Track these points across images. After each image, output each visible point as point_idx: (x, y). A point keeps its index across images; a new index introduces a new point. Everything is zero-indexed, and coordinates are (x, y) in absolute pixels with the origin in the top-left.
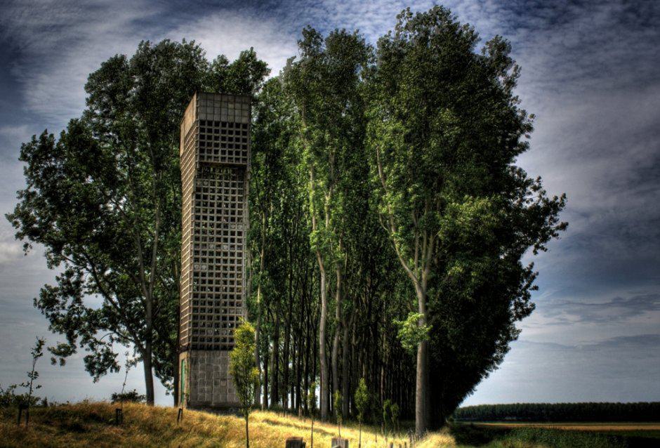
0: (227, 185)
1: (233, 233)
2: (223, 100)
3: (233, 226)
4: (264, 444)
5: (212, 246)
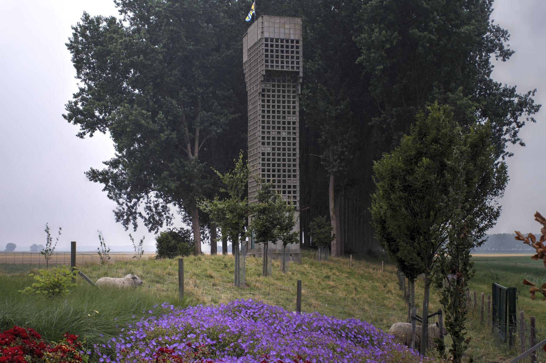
0: (284, 86)
2: (281, 21)
3: (289, 118)
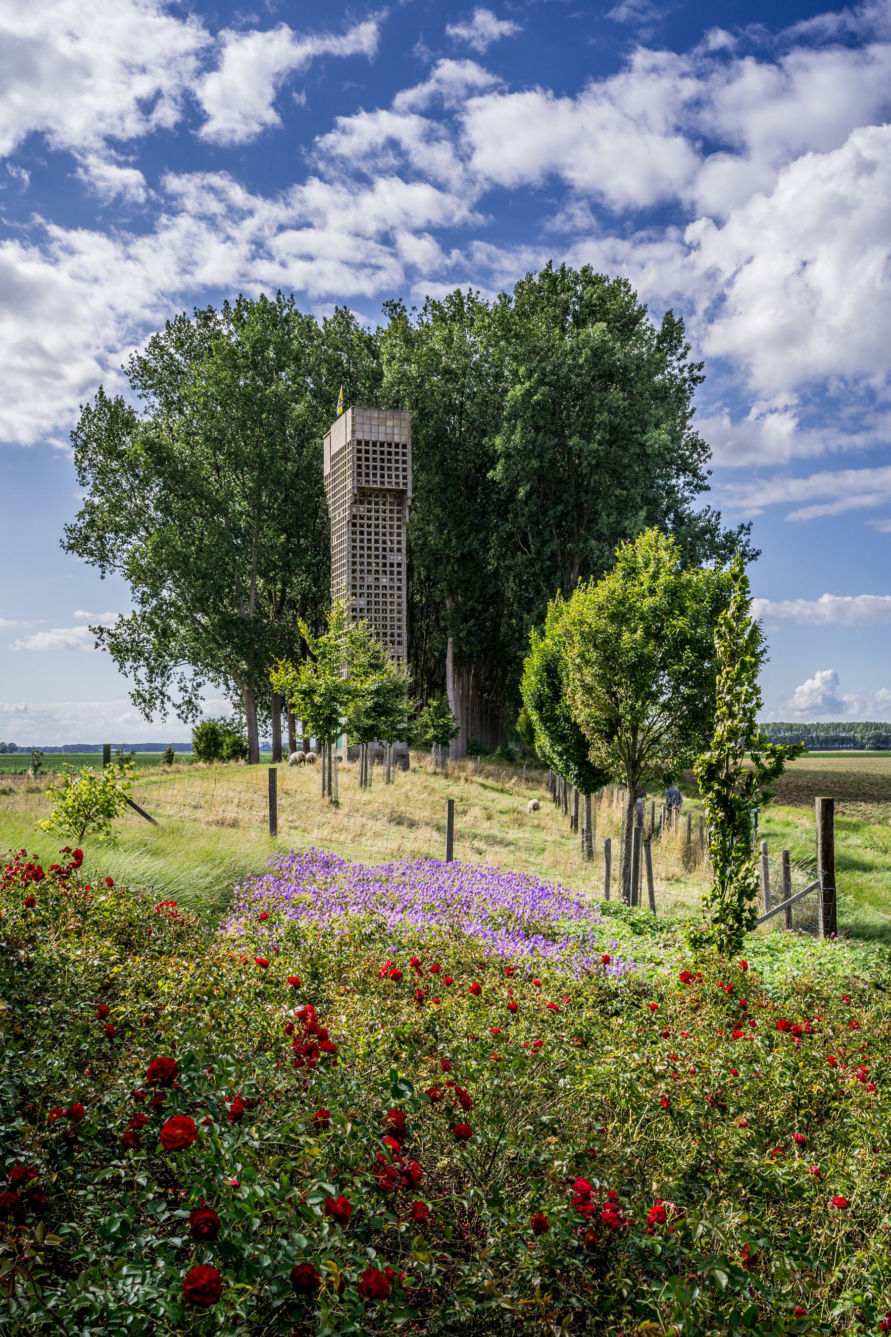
1: (392, 565)
4: (886, 969)
5: (370, 580)
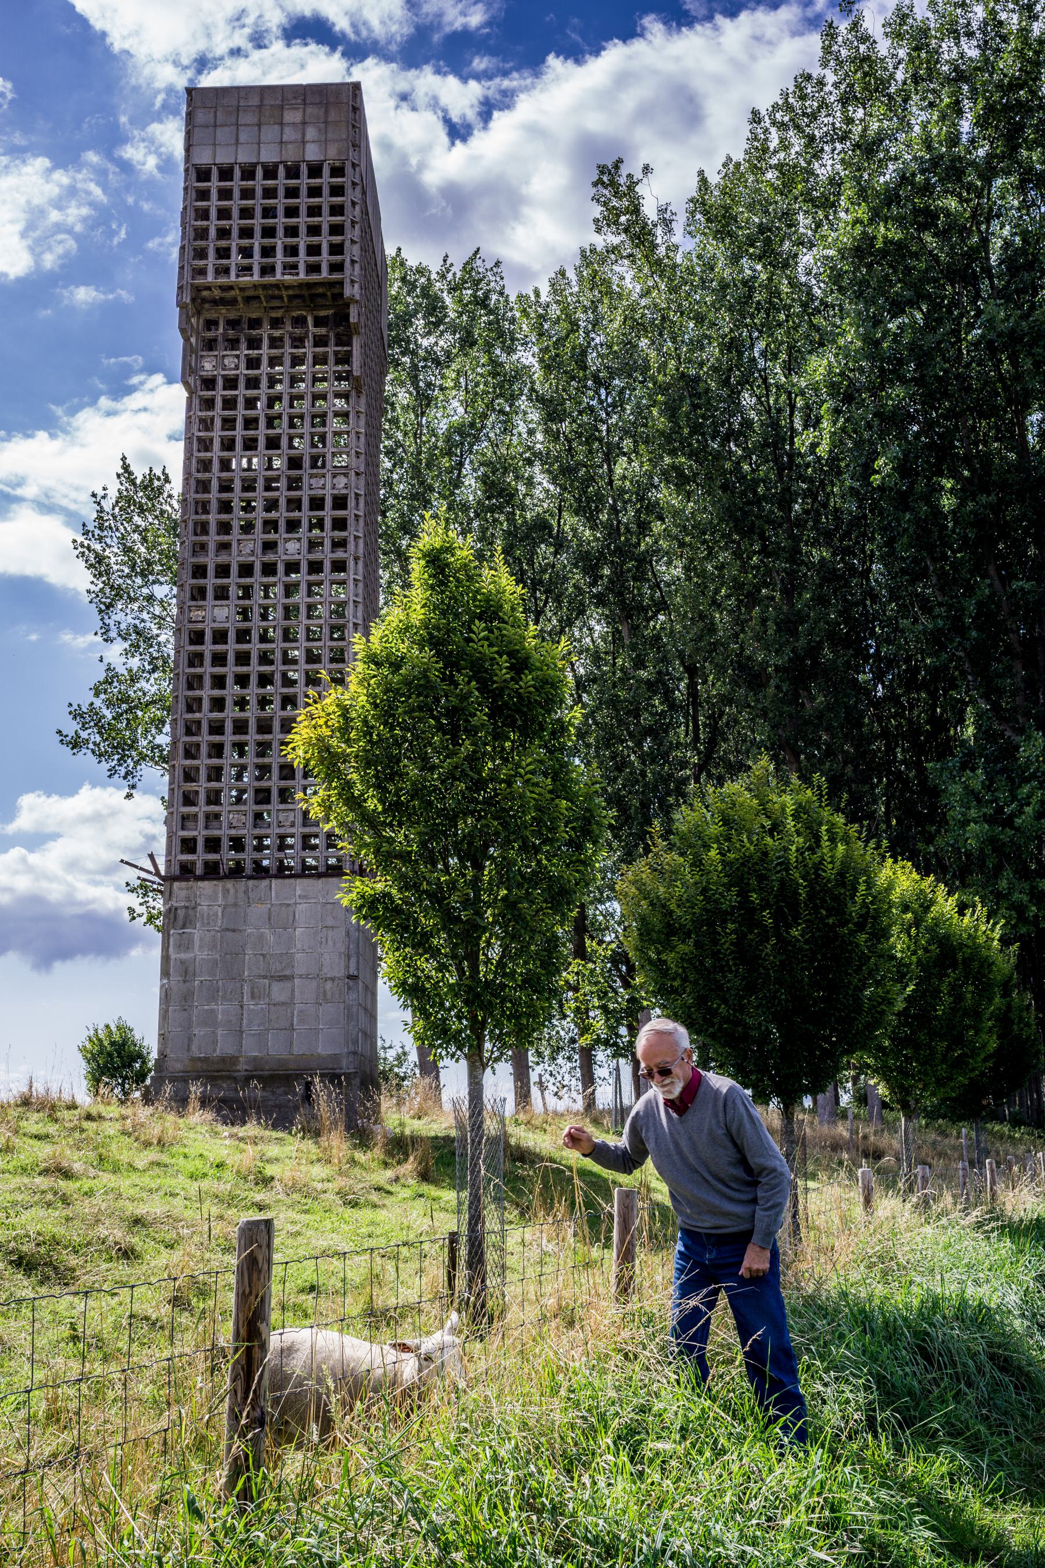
3: (317, 483)
